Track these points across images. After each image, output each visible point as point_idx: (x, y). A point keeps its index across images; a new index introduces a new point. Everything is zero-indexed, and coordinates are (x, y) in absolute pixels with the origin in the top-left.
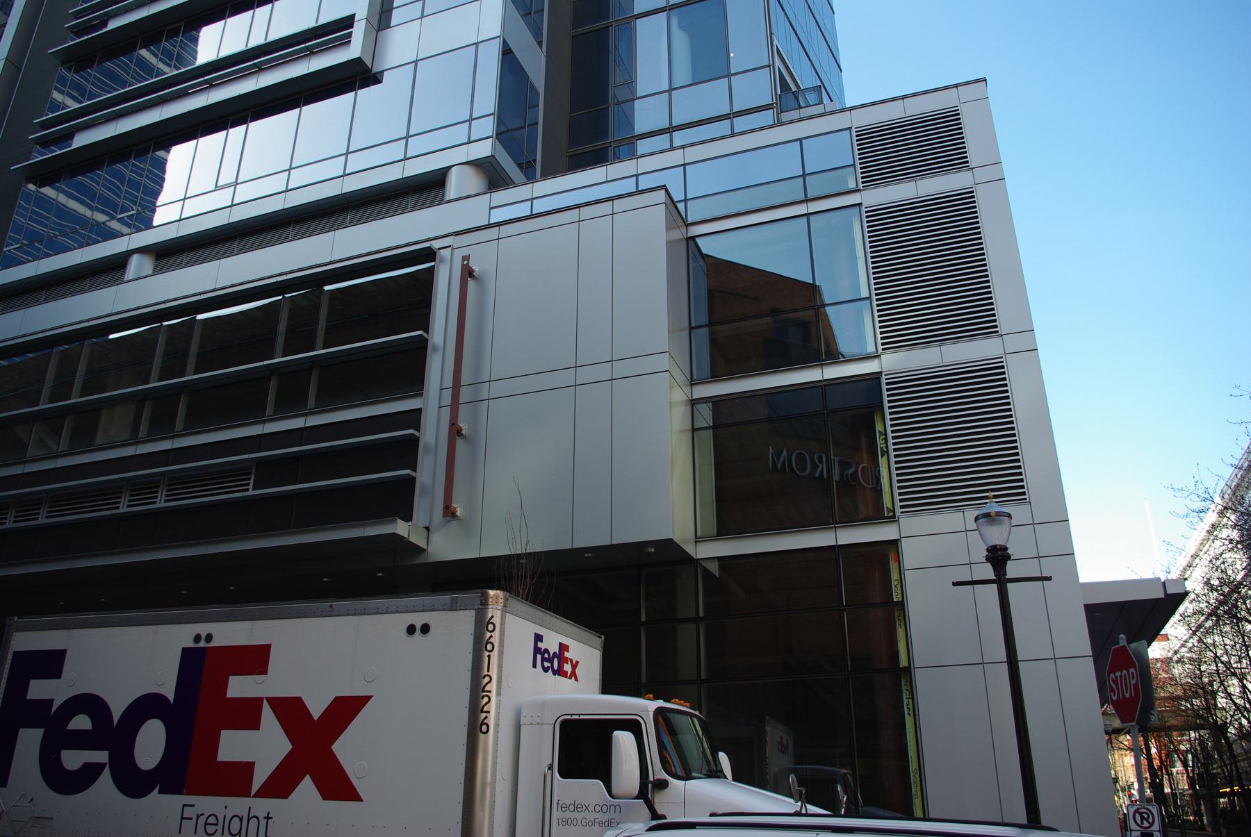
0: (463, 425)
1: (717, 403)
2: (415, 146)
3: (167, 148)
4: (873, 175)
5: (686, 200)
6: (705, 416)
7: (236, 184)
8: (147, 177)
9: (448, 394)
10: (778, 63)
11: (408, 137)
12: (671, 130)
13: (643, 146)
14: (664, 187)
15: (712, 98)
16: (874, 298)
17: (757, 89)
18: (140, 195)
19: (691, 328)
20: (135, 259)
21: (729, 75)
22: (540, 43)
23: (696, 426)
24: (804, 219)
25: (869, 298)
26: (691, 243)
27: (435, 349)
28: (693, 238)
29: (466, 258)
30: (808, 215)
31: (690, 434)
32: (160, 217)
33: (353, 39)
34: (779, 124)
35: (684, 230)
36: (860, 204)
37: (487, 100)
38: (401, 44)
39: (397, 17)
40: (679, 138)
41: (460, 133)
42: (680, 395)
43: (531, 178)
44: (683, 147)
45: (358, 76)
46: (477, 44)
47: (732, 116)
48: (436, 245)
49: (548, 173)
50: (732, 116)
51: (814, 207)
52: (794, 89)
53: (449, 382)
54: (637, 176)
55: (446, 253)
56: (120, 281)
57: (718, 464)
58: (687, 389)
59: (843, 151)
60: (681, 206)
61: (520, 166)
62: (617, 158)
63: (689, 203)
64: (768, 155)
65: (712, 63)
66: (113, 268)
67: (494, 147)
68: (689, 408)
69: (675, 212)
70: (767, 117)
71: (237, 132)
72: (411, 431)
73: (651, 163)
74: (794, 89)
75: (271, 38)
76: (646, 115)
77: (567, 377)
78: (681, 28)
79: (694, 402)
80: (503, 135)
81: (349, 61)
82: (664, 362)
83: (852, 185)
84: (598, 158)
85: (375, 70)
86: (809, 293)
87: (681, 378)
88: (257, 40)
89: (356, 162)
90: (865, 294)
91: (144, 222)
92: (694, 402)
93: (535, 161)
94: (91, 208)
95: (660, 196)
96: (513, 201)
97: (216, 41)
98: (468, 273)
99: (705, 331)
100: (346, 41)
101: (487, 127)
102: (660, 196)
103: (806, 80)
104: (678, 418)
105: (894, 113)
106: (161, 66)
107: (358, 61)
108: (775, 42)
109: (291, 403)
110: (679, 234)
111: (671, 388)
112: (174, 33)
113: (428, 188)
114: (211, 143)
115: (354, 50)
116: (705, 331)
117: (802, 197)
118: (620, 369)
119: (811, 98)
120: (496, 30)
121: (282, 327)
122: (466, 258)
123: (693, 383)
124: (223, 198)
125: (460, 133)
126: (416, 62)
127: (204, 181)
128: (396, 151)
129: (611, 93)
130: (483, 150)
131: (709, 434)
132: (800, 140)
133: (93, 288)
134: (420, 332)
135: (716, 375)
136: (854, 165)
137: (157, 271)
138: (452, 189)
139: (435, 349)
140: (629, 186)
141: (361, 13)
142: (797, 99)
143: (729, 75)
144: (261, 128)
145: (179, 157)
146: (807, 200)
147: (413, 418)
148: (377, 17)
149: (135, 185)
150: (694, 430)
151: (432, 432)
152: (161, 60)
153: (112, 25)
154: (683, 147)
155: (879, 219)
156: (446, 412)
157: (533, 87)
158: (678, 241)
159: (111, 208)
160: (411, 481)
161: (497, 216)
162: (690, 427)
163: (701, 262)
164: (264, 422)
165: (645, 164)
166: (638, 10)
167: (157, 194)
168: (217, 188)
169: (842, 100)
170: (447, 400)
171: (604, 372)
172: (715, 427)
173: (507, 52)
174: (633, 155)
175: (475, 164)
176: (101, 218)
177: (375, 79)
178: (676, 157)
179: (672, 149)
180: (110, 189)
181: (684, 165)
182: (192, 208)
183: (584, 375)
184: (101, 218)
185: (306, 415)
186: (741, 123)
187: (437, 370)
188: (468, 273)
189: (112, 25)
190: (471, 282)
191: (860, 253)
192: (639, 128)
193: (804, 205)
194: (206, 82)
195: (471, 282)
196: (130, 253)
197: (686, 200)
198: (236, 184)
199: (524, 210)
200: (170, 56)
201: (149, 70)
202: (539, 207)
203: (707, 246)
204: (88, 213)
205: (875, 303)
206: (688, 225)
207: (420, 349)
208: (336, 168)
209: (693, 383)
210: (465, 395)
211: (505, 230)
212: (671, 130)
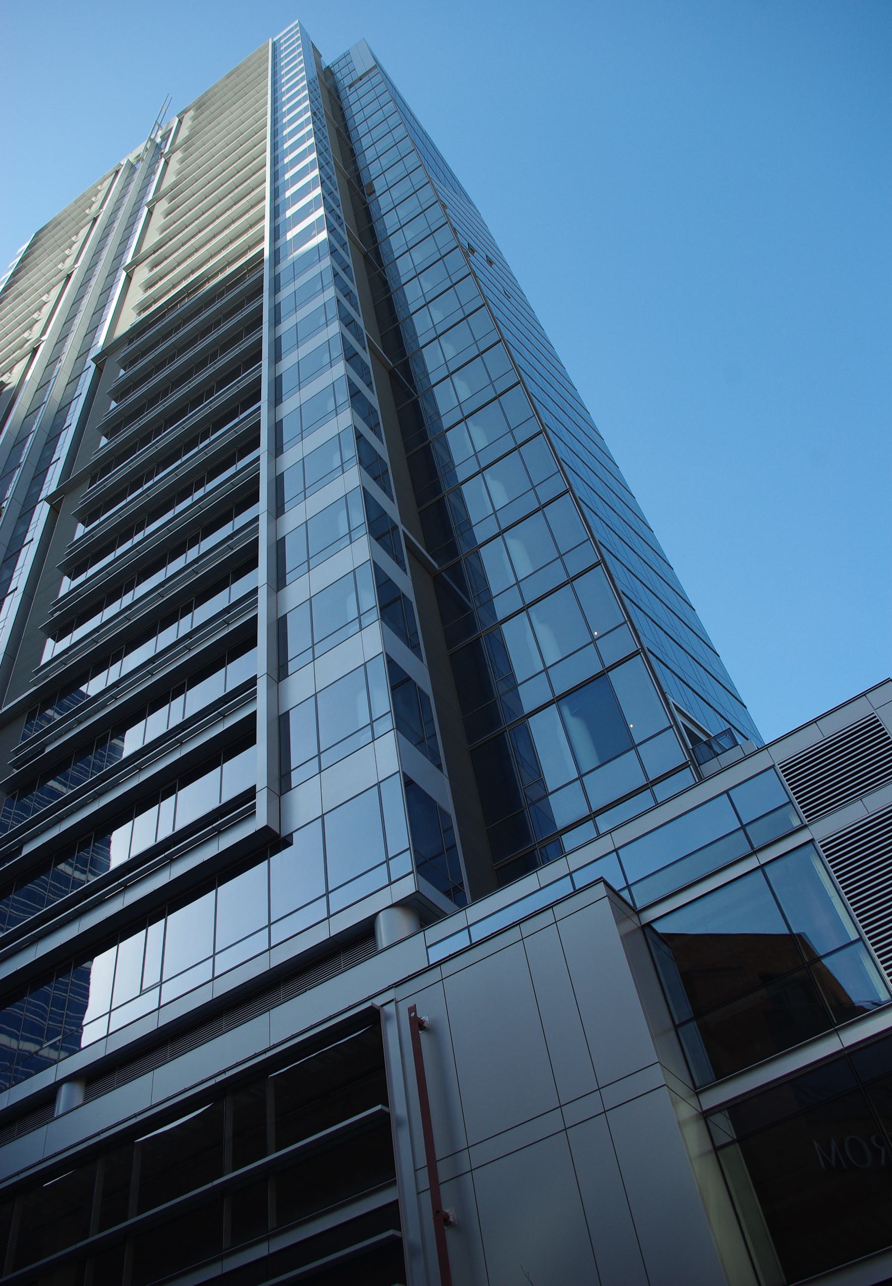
0: (450, 1210)
1: (732, 1107)
2: (338, 900)
3: (92, 960)
4: (816, 806)
5: (628, 887)
6: (725, 1130)
7: (161, 983)
8: (72, 991)
9: (424, 1175)
10: (679, 718)
11: (327, 893)
12: (592, 816)
13: (569, 840)
14: (601, 880)
15: (623, 774)
16: (866, 937)
17: (667, 752)
18: (50, 881)
19: (676, 1027)
20: (64, 1088)
21: (635, 747)
22: (439, 767)
23: (717, 1145)
24: (759, 873)
25: (861, 939)
26: (647, 930)
27: (400, 1123)
28: (649, 925)
29: (412, 1009)
30: (761, 867)
31: (712, 1157)
32: (89, 1036)
33: (257, 809)
34: (701, 779)
35: (635, 918)
36: (812, 841)
37: (400, 836)
38: (304, 803)
39: (296, 778)
40: (604, 822)
41: (379, 877)
42: (686, 1110)
43: (462, 904)
44: (610, 832)
45: (269, 843)
46: (378, 784)
47: (650, 785)
48: (378, 1002)
49: (480, 894)
50: (650, 785)
51: (766, 856)
52: (705, 739)
53: (422, 1161)
54: (570, 874)
55: (390, 1009)
56: (50, 1118)
57: (758, 1184)
58: (693, 1101)
59: (773, 792)
60: (625, 894)
61: (447, 893)
62: (547, 860)
63: (632, 888)
64: (696, 815)
65: (613, 739)
66: (46, 1100)
67: (417, 883)
68: (702, 1123)
69: (622, 904)
70: (687, 777)
71: (156, 929)
72: (379, 1107)
73: (583, 856)
74: (705, 739)
75: (179, 826)
76: (564, 808)
77: (553, 1122)
78: (574, 715)
79: (706, 1115)
80: (424, 866)
81: (257, 832)
82: (656, 1076)
83: (796, 823)
84: (527, 865)
85: (283, 834)
86: (793, 945)
87: (682, 1089)
88: (166, 832)
89: (280, 932)
90: (854, 936)
91: (72, 1043)
92: (706, 1115)
93: (462, 884)
94: (16, 1037)
95: (601, 889)
96: (448, 935)
97: (125, 844)
98: (417, 1025)
99: (693, 1025)
100: (251, 813)
101: (406, 863)
102: (601, 889)
103: (714, 726)
104: (694, 1140)
105: (812, 738)
106: (77, 875)
107: (266, 829)
108: (671, 700)
109: (251, 1228)
110: (631, 924)
111: (674, 1104)
112: (85, 845)
113: (359, 940)
114: (131, 946)
115: (260, 820)
116: (693, 1025)
117: (748, 850)
118: (611, 1096)
119: (725, 742)
120: (395, 767)
121: (228, 1133)
122: (412, 1009)
123: (697, 1091)
124: (149, 1002)
125: (379, 877)
126: (322, 816)
127: (128, 987)
128: (319, 911)
129: (522, 796)
130: (407, 887)
131: (736, 1149)
132: (726, 792)
133: (21, 1133)
134: (379, 1107)
135: (723, 1073)
136: (790, 802)
137: (88, 1098)
138: (384, 937)
139: (400, 1123)
140: (565, 887)
141: (261, 783)
142: (711, 747)
143: (635, 747)
144: (179, 920)
145: (101, 967)
146: (755, 852)
147: (390, 1215)
148: (277, 783)
149: (59, 1003)
150: (716, 1149)
151: (415, 1227)
152: (76, 869)
153: (26, 850)
154: (610, 832)
155: (838, 850)
156: (427, 1197)
157: (443, 812)
158: (633, 932)
159: (37, 1033)
160: (396, 1244)
161: (437, 954)
162: (710, 1147)
163: (664, 947)
164: (221, 1259)
165: (575, 860)
166: (527, 709)
167: (84, 1008)
168: (142, 992)
169: (759, 738)
170: (425, 1183)
171: (592, 1105)
172: (742, 1138)
173: (409, 784)
174: (561, 853)
175: (402, 904)
176: (31, 1047)
177: (285, 842)
178: (605, 845)
179: (600, 836)
180: (34, 1013)
181: (616, 850)
182: (119, 1019)
183: (573, 1113)
184: (31, 1047)
185: (268, 1238)
186: (662, 791)
187: (407, 1148)
188: (417, 1025)
189: (26, 850)
190: (423, 1035)
191: (832, 892)
192: (561, 822)
193: (754, 858)
194: (120, 885)
195: (423, 1035)
196: (57, 1085)
197: (628, 887)
198: (161, 983)
199: (461, 941)
200: (84, 862)
201: (55, 794)
202: (478, 933)
203: (661, 927)
204: (13, 1044)
205: (869, 943)
206: (638, 912)
207: (381, 1129)
208: (259, 943)
209: (697, 1091)
210: (444, 1172)
211: (447, 968)
212: (592, 816)
